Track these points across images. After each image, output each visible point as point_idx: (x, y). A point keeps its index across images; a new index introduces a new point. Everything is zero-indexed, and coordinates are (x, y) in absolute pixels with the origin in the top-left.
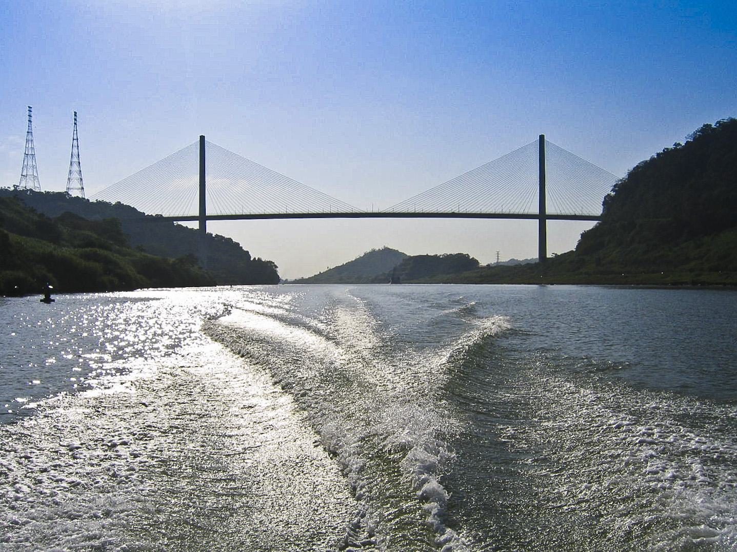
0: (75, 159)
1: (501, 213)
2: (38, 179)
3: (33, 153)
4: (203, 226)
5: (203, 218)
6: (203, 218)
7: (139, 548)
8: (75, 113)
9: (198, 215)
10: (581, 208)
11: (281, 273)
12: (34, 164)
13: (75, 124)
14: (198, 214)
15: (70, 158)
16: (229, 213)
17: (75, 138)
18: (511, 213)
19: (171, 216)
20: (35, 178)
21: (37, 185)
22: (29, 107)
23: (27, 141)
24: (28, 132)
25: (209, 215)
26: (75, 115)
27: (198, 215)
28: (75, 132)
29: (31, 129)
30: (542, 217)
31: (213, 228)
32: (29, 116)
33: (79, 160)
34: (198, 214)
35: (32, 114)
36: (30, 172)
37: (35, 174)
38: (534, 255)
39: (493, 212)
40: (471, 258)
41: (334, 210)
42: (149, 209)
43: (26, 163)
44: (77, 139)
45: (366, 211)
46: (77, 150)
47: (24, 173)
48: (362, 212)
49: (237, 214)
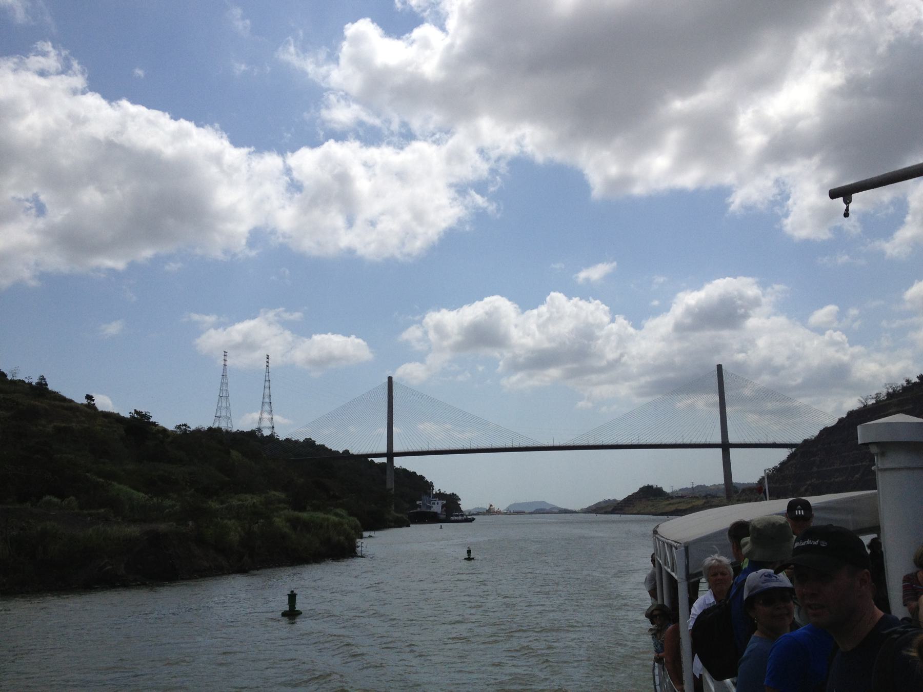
0: (267, 400)
1: (682, 443)
2: (231, 420)
3: (227, 395)
4: (390, 461)
5: (390, 455)
6: (390, 455)
7: (540, 690)
8: (268, 356)
9: (394, 458)
10: (427, 443)
11: (466, 505)
12: (228, 405)
13: (267, 366)
14: (731, 450)
15: (262, 399)
16: (420, 450)
17: (267, 379)
18: (663, 443)
19: (360, 453)
20: (228, 418)
21: (230, 425)
22: (225, 352)
23: (222, 383)
24: (223, 376)
25: (396, 452)
26: (268, 358)
27: (394, 458)
28: (267, 374)
29: (226, 372)
30: (725, 446)
31: (398, 462)
32: (224, 360)
33: (270, 400)
34: (731, 450)
35: (266, 364)
36: (224, 414)
37: (229, 415)
38: (720, 480)
39: (659, 443)
40: (459, 503)
41: (425, 448)
42: (337, 445)
43: (219, 405)
44: (265, 381)
45: (547, 445)
46: (268, 391)
47: (218, 415)
48: (543, 445)
49: (423, 450)
